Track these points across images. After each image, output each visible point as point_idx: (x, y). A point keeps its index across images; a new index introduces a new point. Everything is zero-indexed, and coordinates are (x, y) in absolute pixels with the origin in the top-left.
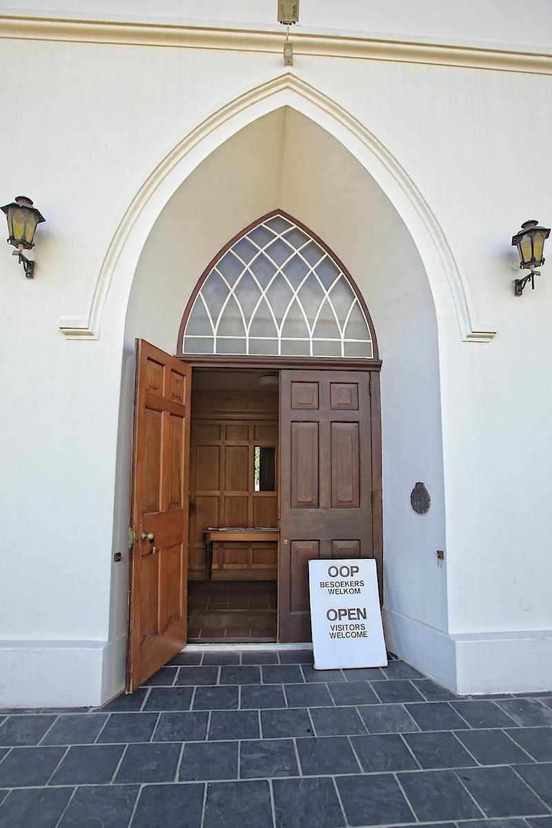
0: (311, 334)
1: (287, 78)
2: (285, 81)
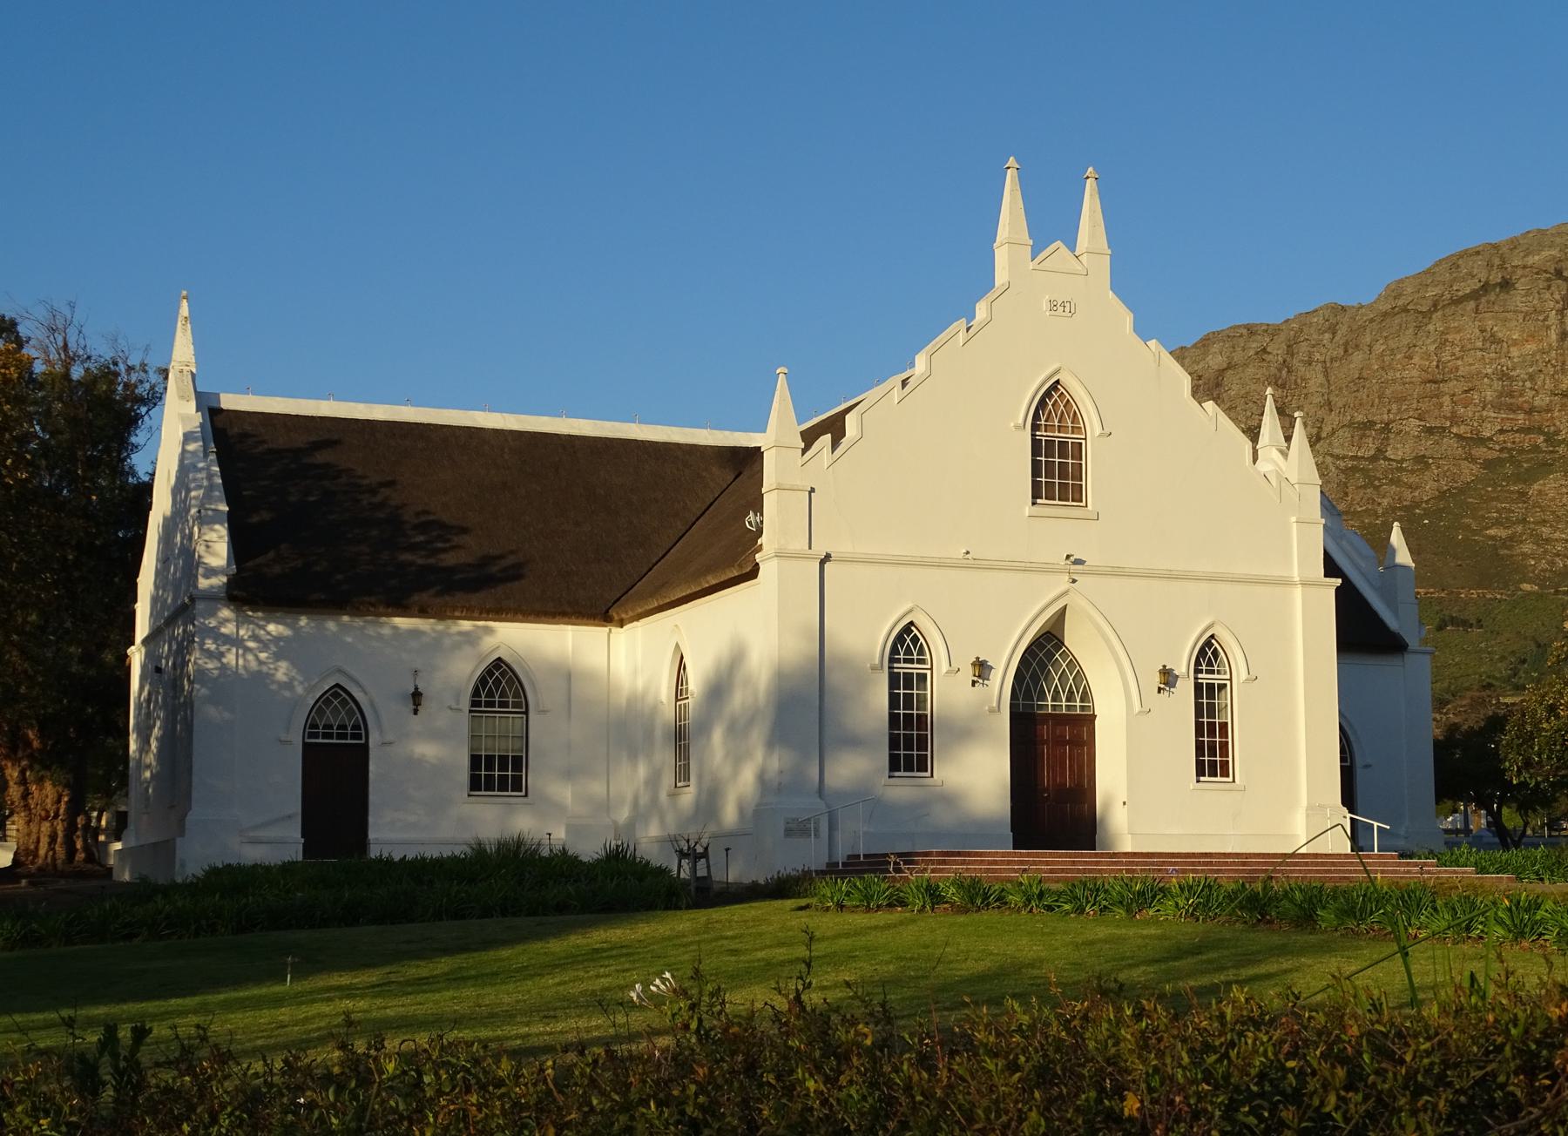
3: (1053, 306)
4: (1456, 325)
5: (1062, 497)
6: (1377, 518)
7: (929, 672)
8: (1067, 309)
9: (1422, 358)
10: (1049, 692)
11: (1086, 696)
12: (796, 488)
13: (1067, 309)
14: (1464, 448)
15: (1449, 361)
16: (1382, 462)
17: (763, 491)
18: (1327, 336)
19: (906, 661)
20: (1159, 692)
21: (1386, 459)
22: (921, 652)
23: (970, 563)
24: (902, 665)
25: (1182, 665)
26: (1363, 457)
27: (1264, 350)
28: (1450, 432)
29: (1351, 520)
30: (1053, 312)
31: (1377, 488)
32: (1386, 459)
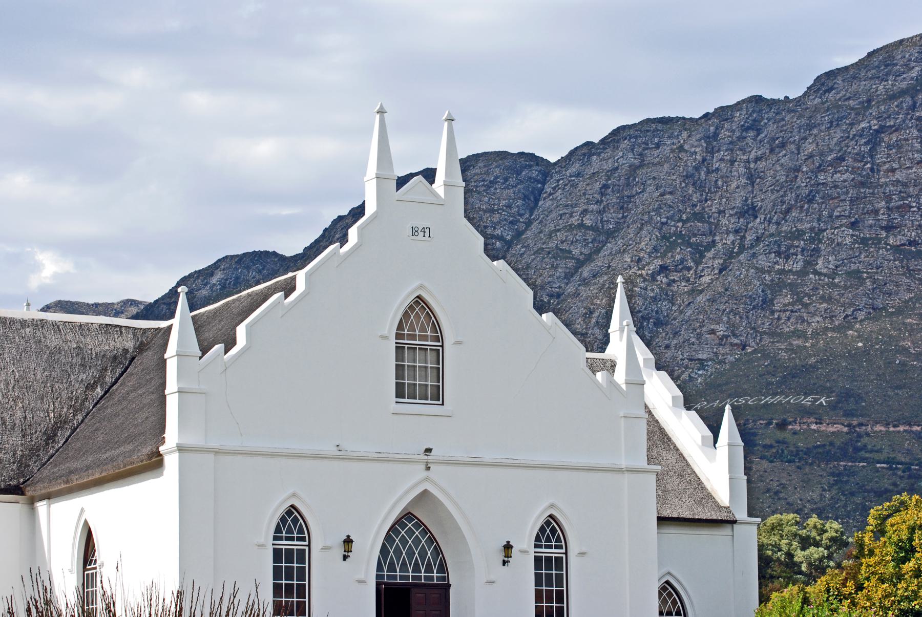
0: (423, 572)
1: (427, 479)
2: (427, 479)
3: (415, 231)
4: (892, 123)
5: (424, 388)
6: (806, 339)
7: (307, 548)
8: (427, 234)
9: (855, 160)
10: (410, 565)
11: (443, 568)
12: (194, 391)
13: (427, 234)
14: (901, 261)
15: (885, 163)
16: (811, 276)
17: (167, 392)
18: (751, 134)
19: (287, 539)
20: (504, 564)
21: (816, 273)
22: (301, 531)
23: (343, 456)
24: (284, 542)
25: (525, 543)
26: (790, 271)
27: (681, 149)
28: (886, 243)
29: (777, 342)
30: (414, 237)
31: (806, 306)
32: (816, 273)
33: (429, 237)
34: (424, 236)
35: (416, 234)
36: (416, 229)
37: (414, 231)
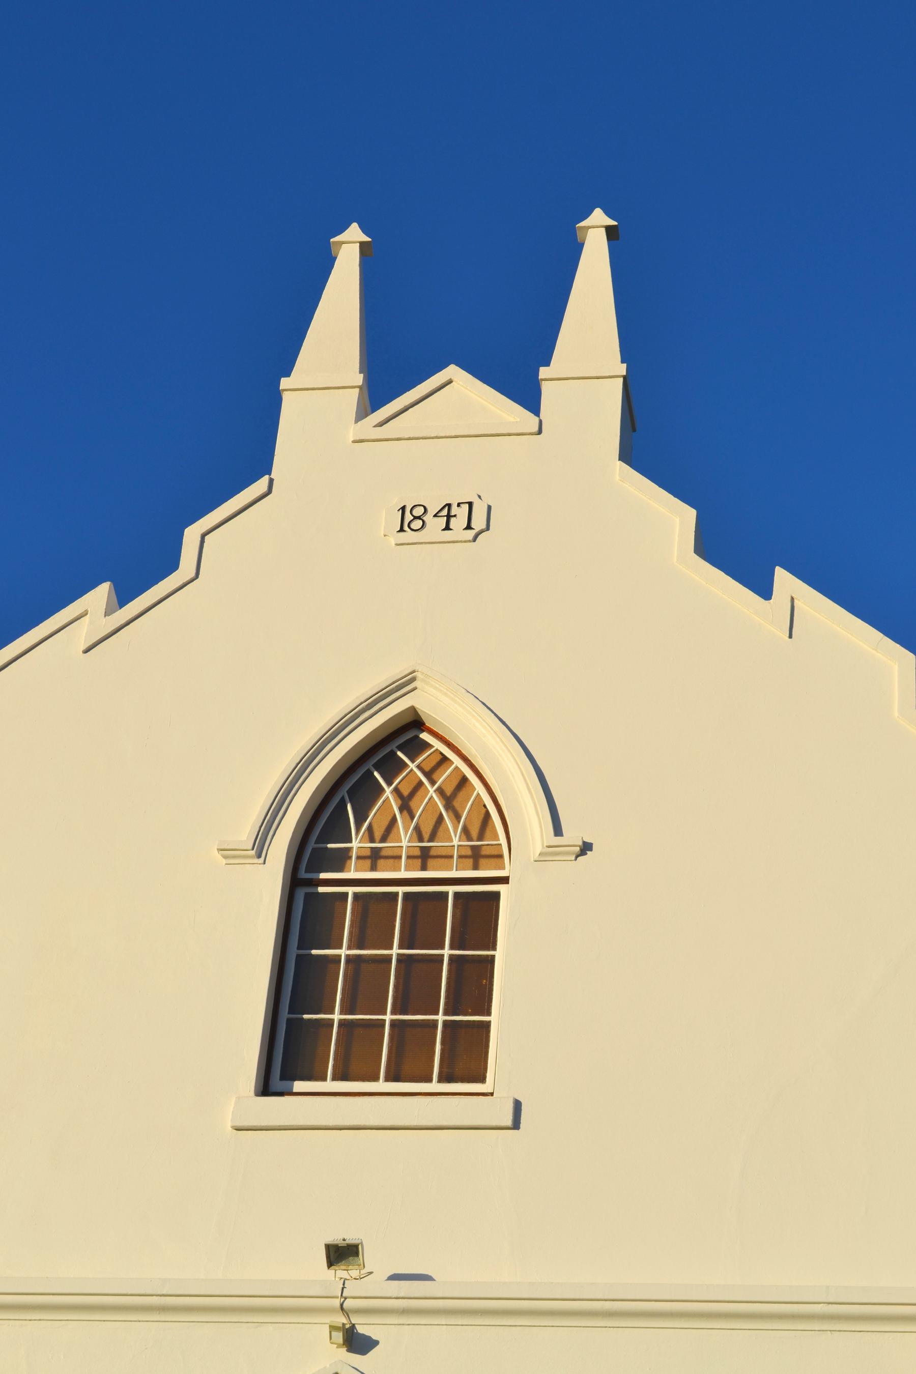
13: (459, 523)
30: (409, 536)
33: (469, 527)
34: (447, 528)
35: (417, 524)
36: (419, 511)
37: (408, 517)
